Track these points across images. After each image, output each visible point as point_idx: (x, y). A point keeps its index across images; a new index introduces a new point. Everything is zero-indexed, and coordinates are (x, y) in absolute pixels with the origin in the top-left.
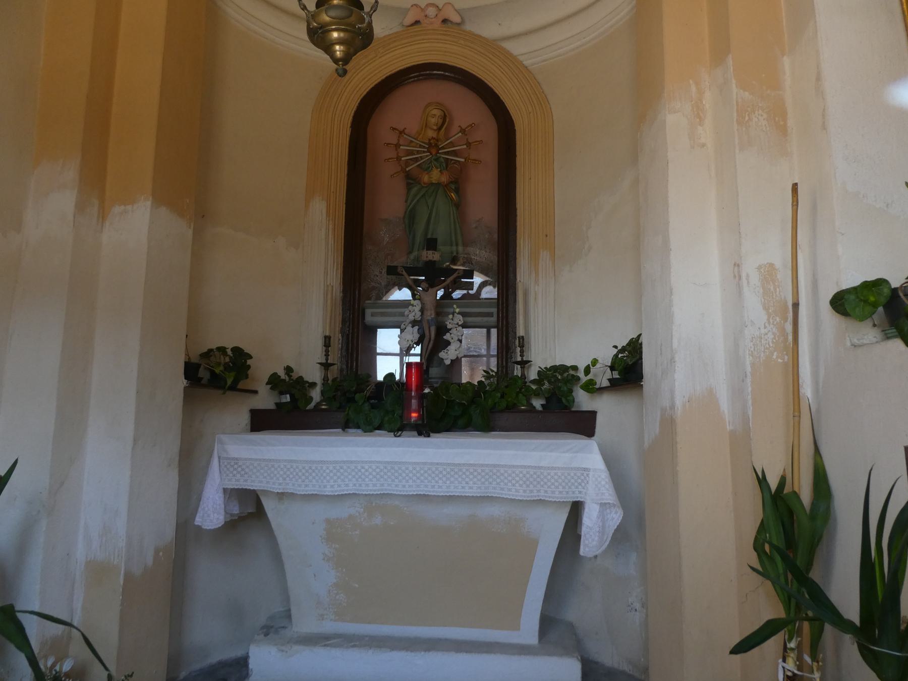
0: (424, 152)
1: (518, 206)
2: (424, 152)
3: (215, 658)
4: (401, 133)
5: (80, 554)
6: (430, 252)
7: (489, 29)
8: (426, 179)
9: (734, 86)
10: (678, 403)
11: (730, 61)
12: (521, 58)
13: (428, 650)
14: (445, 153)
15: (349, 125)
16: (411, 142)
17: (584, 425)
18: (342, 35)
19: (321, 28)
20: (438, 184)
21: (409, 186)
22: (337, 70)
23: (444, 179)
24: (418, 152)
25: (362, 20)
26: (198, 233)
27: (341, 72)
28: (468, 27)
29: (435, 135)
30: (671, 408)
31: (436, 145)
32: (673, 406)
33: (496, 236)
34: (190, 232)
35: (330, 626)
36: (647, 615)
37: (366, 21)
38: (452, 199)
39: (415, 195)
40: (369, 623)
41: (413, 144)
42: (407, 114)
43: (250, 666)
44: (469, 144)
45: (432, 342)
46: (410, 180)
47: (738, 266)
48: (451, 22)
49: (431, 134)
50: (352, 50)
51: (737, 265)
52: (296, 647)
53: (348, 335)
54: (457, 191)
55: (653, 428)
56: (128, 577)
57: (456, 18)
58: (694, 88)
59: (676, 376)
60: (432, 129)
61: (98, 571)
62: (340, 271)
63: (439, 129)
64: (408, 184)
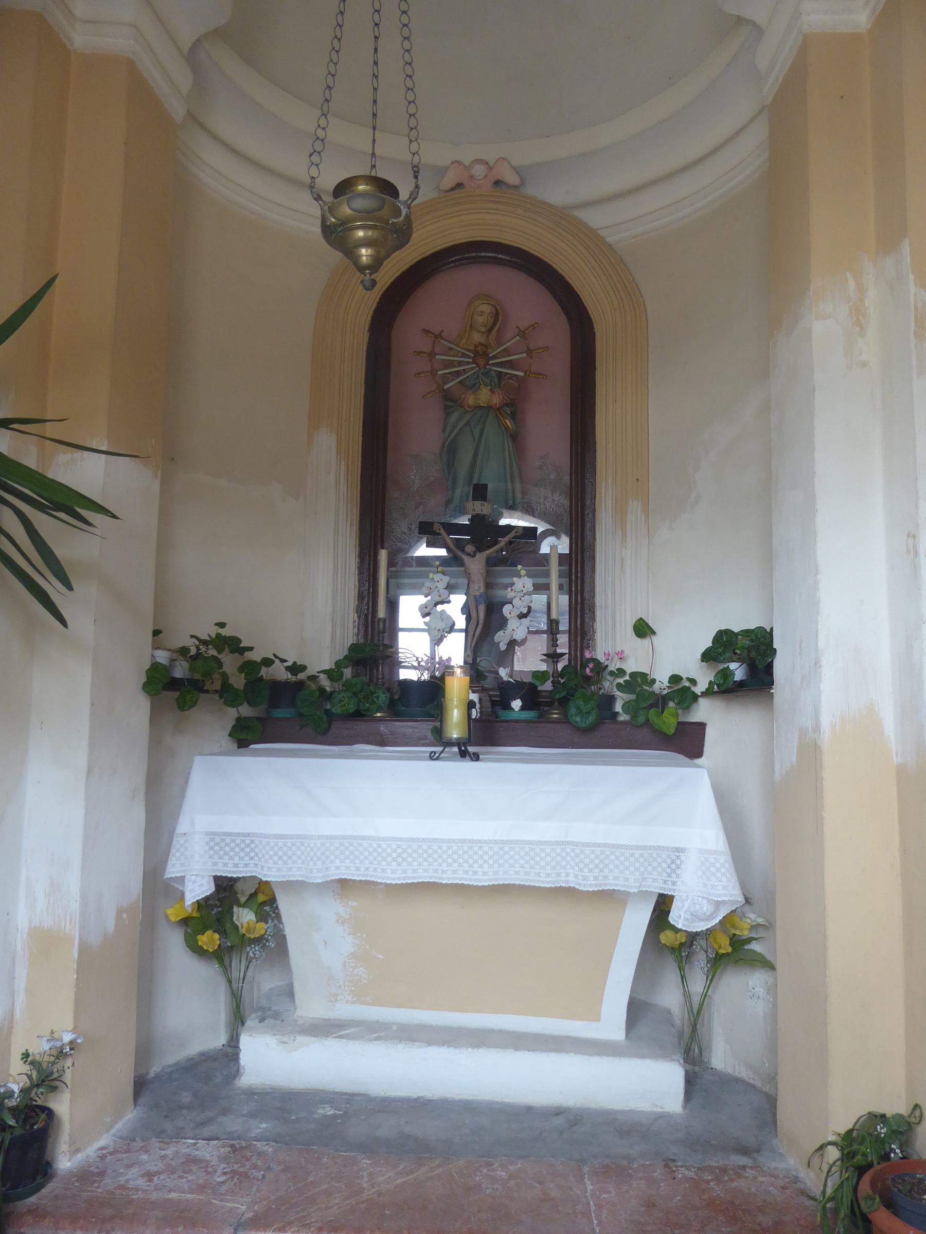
0: (468, 363)
1: (598, 439)
2: (468, 363)
3: (194, 1049)
4: (436, 337)
5: (23, 919)
6: (478, 503)
7: (556, 194)
8: (471, 400)
9: (912, 284)
10: (825, 722)
11: (906, 247)
12: (602, 233)
13: (476, 1046)
14: (497, 365)
15: (367, 328)
16: (451, 349)
17: (688, 742)
18: (370, 233)
19: (341, 225)
20: (489, 408)
21: (448, 411)
22: (362, 282)
23: (496, 400)
24: (460, 363)
25: (398, 212)
26: (166, 482)
27: (368, 284)
28: (532, 190)
29: (483, 341)
30: (814, 731)
31: (485, 354)
32: (817, 728)
33: (567, 479)
34: (156, 486)
35: (345, 1010)
36: (775, 1005)
37: (404, 212)
38: (507, 428)
39: (454, 427)
40: (398, 1007)
41: (452, 353)
42: (443, 308)
43: (242, 1062)
44: (529, 352)
45: (480, 626)
46: (450, 402)
47: (914, 537)
48: (506, 184)
49: (477, 338)
50: (383, 252)
51: (912, 536)
52: (301, 1039)
53: (366, 616)
54: (513, 416)
55: (788, 754)
56: (84, 949)
57: (513, 179)
58: (852, 284)
59: (822, 686)
60: (479, 332)
61: (44, 941)
62: (355, 528)
63: (489, 331)
64: (446, 407)
